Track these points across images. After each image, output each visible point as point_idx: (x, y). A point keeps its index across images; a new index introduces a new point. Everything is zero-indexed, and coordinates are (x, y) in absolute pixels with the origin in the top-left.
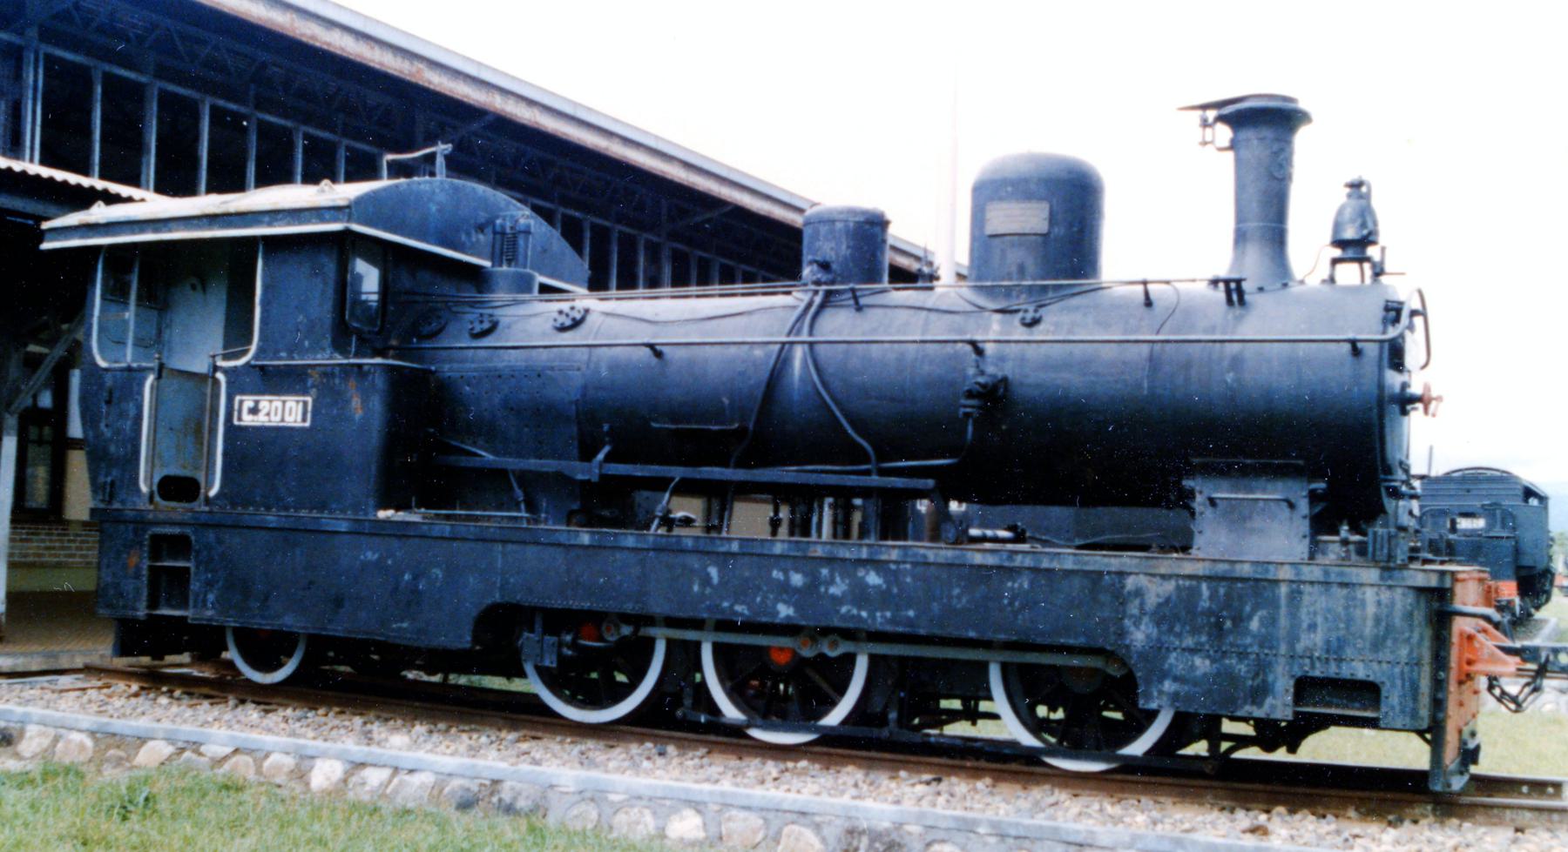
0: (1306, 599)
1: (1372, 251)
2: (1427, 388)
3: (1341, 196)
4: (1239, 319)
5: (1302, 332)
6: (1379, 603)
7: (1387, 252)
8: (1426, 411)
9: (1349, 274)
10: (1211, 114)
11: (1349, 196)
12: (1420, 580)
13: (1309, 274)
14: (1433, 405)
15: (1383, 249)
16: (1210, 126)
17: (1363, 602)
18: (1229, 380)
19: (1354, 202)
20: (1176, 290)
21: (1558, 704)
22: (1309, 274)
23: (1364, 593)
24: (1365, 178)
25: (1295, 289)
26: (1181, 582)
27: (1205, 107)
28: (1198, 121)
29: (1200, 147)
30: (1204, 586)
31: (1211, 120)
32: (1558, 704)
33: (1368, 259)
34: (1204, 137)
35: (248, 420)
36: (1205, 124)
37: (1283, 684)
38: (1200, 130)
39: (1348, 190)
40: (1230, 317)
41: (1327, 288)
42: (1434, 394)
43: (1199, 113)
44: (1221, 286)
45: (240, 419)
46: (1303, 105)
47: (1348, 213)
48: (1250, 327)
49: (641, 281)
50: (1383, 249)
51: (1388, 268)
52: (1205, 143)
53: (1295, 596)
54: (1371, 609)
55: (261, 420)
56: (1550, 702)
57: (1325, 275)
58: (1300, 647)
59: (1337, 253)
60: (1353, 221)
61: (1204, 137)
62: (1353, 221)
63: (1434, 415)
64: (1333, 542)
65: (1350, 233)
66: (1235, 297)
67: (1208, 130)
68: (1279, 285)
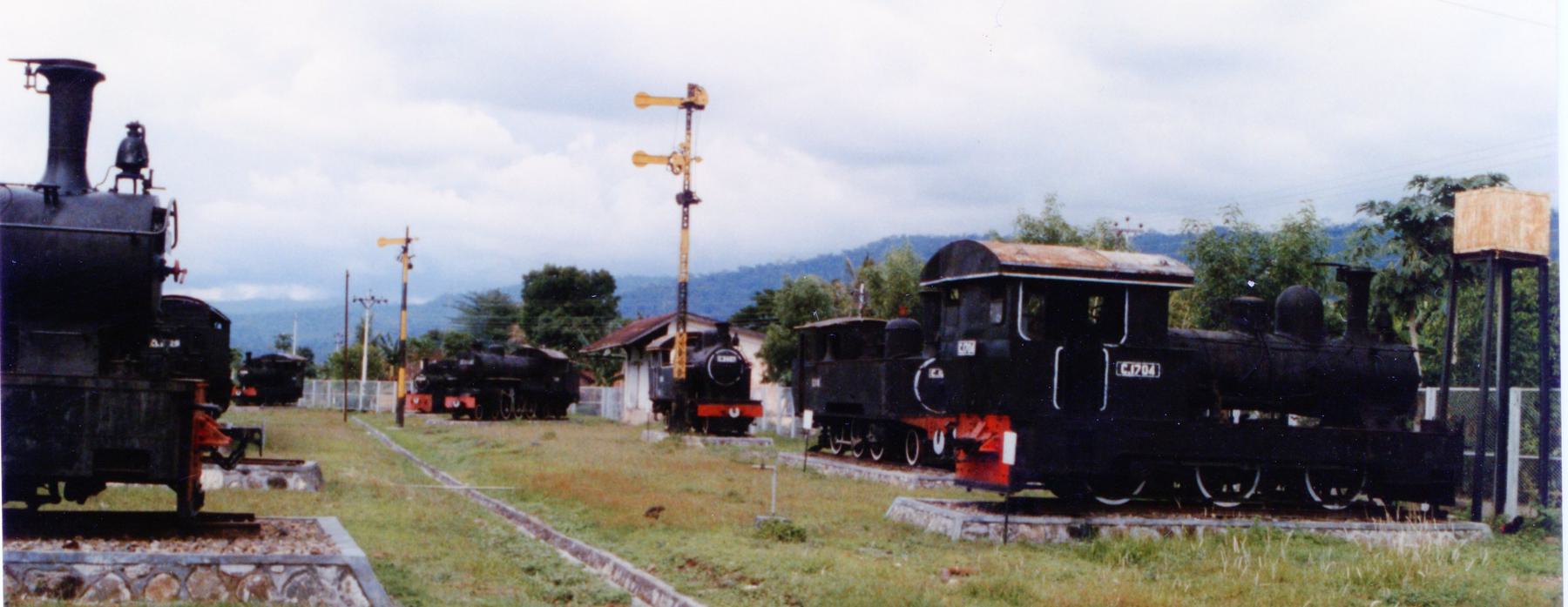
0: (102, 400)
1: (144, 172)
2: (177, 264)
3: (123, 133)
4: (54, 213)
5: (98, 226)
6: (149, 402)
7: (154, 174)
8: (176, 279)
9: (126, 186)
10: (34, 67)
11: (129, 134)
12: (175, 388)
13: (102, 183)
14: (180, 276)
15: (151, 172)
16: (35, 75)
17: (139, 403)
18: (47, 255)
19: (132, 139)
20: (10, 190)
21: (241, 482)
22: (102, 183)
23: (140, 396)
24: (141, 123)
25: (91, 195)
26: (16, 390)
27: (29, 61)
28: (23, 71)
29: (25, 89)
30: (33, 393)
31: (33, 71)
32: (241, 482)
33: (142, 177)
34: (28, 82)
35: (1124, 373)
36: (29, 72)
37: (86, 454)
38: (25, 77)
39: (128, 130)
40: (47, 212)
41: (112, 194)
42: (182, 267)
43: (25, 64)
44: (42, 190)
45: (1119, 372)
46: (99, 69)
47: (129, 145)
48: (61, 221)
49: (598, 403)
50: (151, 172)
51: (155, 183)
52: (28, 86)
53: (95, 399)
54: (144, 406)
55: (1131, 374)
56: (235, 481)
57: (112, 186)
58: (98, 431)
59: (119, 171)
60: (132, 151)
61: (28, 82)
62: (132, 151)
63: (181, 282)
64: (120, 364)
65: (129, 159)
66: (51, 198)
67: (32, 78)
68: (80, 191)
